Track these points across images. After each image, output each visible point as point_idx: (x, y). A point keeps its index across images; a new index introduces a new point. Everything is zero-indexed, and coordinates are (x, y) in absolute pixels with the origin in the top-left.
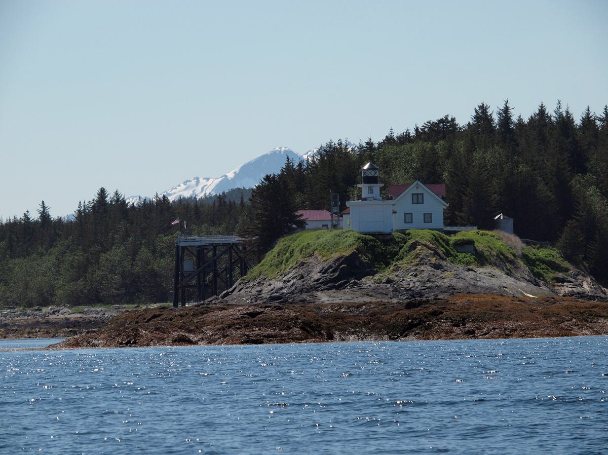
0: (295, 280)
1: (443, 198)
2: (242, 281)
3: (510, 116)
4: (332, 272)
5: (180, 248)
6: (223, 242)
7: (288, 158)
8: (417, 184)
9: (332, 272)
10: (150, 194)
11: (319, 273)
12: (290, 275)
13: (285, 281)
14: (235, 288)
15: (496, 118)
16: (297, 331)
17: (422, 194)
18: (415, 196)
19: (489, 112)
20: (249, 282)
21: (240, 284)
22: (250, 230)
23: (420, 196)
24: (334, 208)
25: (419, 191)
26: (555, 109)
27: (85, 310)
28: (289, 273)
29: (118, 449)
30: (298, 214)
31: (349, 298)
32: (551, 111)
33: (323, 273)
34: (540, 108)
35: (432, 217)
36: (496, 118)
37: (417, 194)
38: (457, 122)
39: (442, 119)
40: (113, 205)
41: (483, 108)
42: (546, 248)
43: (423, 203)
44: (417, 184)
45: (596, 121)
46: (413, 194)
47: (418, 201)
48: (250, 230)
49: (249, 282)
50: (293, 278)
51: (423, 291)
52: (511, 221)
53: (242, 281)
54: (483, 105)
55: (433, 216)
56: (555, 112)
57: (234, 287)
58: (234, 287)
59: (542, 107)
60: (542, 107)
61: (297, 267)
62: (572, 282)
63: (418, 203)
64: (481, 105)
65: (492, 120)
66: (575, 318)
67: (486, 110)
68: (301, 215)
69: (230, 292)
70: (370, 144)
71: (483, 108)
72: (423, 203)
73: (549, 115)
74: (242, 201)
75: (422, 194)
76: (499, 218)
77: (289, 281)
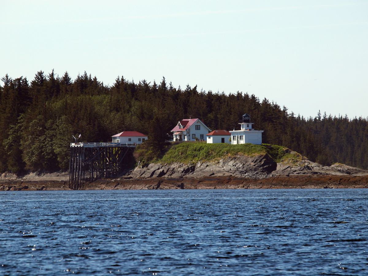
7: (90, 75)
10: (314, 116)
16: (266, 266)
17: (200, 126)
19: (44, 75)
23: (199, 126)
29: (127, 254)
34: (117, 80)
35: (195, 128)
37: (198, 125)
38: (148, 82)
41: (40, 74)
43: (200, 130)
45: (175, 94)
47: (198, 127)
55: (195, 129)
59: (66, 73)
60: (66, 73)
63: (198, 130)
66: (239, 152)
70: (66, 78)
71: (40, 74)
72: (200, 130)
75: (200, 126)
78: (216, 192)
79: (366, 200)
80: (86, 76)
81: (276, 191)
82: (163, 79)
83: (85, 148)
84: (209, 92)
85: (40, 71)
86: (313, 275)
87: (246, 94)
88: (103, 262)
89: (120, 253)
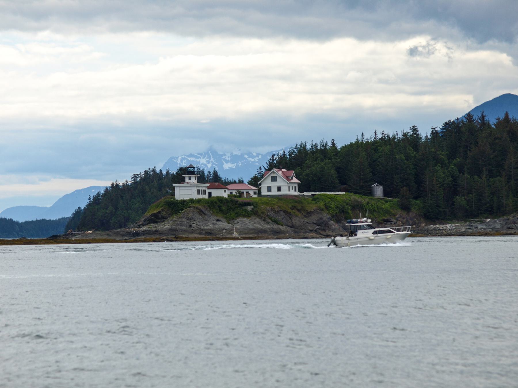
8: (273, 171)
17: (276, 176)
23: (275, 178)
25: (275, 175)
44: (273, 171)
46: (272, 177)
63: (274, 181)
75: (276, 176)
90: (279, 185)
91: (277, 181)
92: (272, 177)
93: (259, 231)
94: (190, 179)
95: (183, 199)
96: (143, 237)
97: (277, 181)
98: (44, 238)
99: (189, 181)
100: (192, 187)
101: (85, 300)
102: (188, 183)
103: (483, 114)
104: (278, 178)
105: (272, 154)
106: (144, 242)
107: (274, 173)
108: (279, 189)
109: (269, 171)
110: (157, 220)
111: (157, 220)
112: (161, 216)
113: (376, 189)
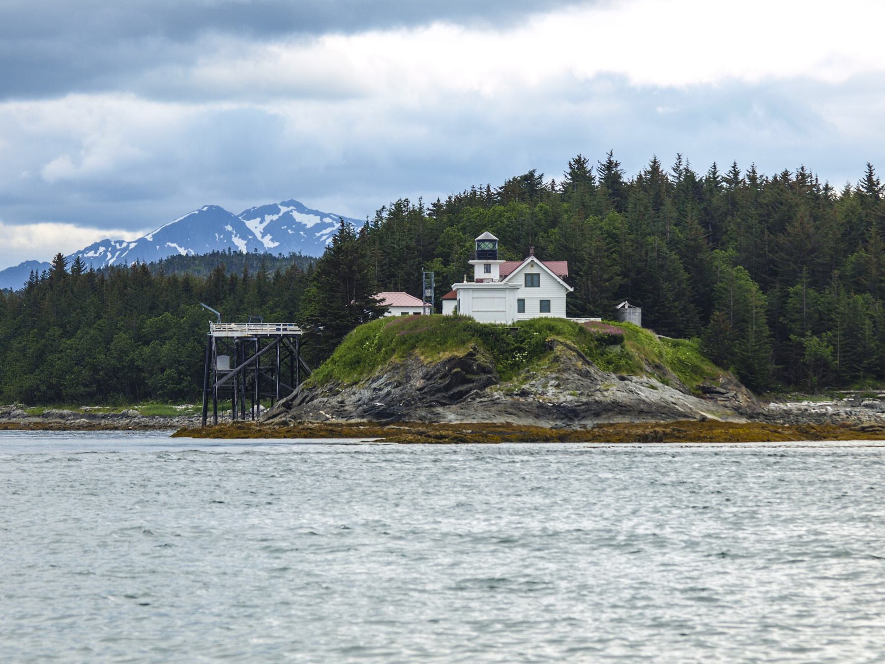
0: (389, 388)
1: (565, 279)
2: (305, 386)
3: (753, 177)
4: (441, 378)
5: (214, 340)
6: (271, 333)
7: (715, 166)
8: (532, 261)
9: (441, 378)
11: (423, 378)
12: (382, 381)
13: (375, 389)
14: (296, 396)
15: (597, 176)
17: (538, 275)
18: (529, 278)
19: (588, 166)
20: (314, 387)
21: (303, 390)
22: (314, 318)
23: (535, 278)
24: (426, 291)
25: (535, 271)
26: (674, 165)
27: (45, 412)
28: (379, 378)
30: (378, 299)
31: (485, 417)
32: (667, 169)
33: (428, 380)
36: (597, 176)
39: (526, 176)
40: (427, 316)
42: (608, 335)
43: (539, 286)
44: (532, 261)
46: (526, 275)
48: (314, 318)
49: (314, 387)
50: (386, 385)
51: (578, 408)
52: (639, 310)
53: (305, 386)
54: (580, 158)
56: (674, 169)
57: (295, 393)
58: (295, 393)
59: (655, 162)
60: (655, 162)
61: (389, 371)
62: (723, 394)
63: (532, 286)
64: (577, 158)
65: (591, 179)
67: (582, 165)
68: (384, 300)
69: (290, 400)
73: (664, 173)
74: (246, 276)
75: (538, 275)
76: (624, 307)
77: (380, 390)
78: (38, 463)
79: (279, 491)
80: (735, 170)
81: (41, 460)
82: (868, 171)
83: (216, 337)
84: (532, 174)
85: (577, 158)
86: (534, 659)
87: (537, 175)
88: (492, 588)
89: (723, 557)
90: (545, 297)
91: (539, 286)
92: (526, 275)
93: (398, 418)
94: (488, 269)
95: (493, 322)
96: (589, 423)
97: (539, 286)
98: (626, 420)
99: (487, 276)
100: (507, 292)
101: (324, 585)
102: (481, 281)
103: (611, 159)
104: (543, 279)
105: (784, 171)
106: (817, 437)
107: (532, 266)
108: (545, 305)
109: (518, 263)
110: (469, 376)
111: (469, 376)
112: (478, 365)
113: (630, 315)
